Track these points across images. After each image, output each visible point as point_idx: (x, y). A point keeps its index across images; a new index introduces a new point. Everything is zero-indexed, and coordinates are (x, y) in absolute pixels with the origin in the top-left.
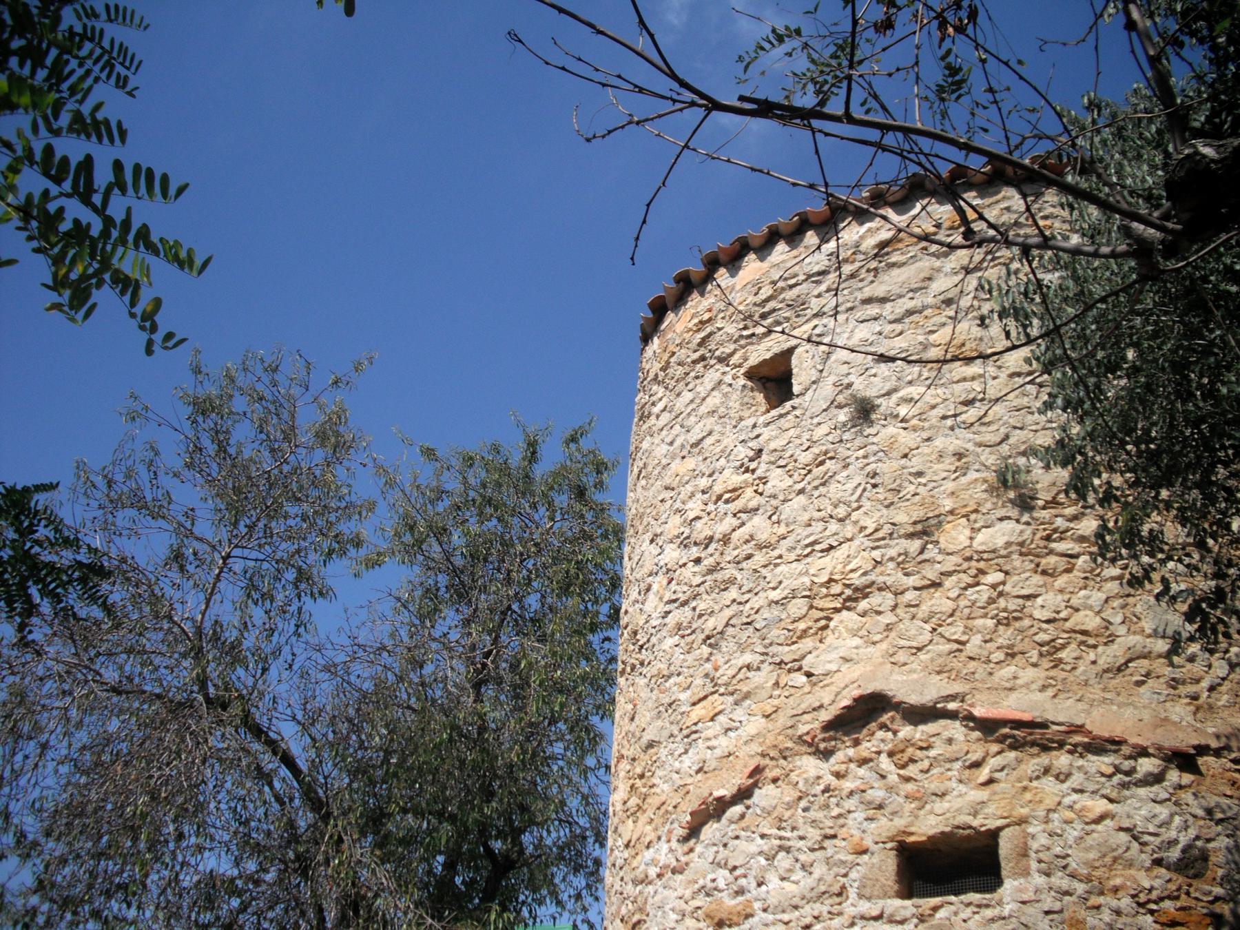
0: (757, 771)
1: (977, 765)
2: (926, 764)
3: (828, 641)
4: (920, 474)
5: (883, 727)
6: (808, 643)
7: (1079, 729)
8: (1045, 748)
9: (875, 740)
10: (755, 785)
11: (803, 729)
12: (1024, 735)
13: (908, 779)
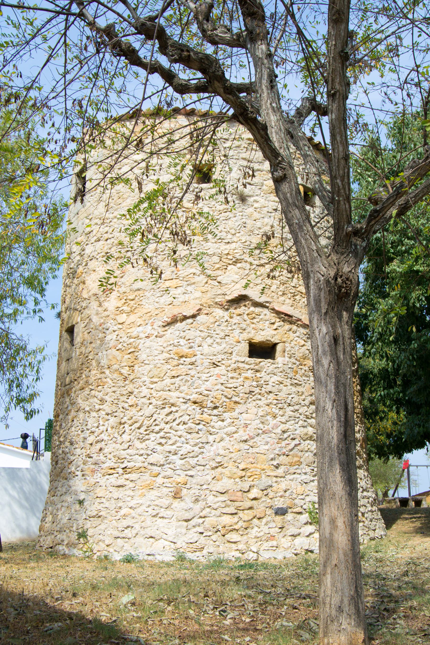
0: (200, 310)
1: (273, 324)
2: (258, 320)
3: (227, 273)
4: (260, 228)
5: (245, 306)
6: (219, 272)
7: (300, 320)
8: (291, 323)
9: (242, 310)
10: (198, 314)
11: (217, 300)
12: (287, 318)
13: (253, 323)
